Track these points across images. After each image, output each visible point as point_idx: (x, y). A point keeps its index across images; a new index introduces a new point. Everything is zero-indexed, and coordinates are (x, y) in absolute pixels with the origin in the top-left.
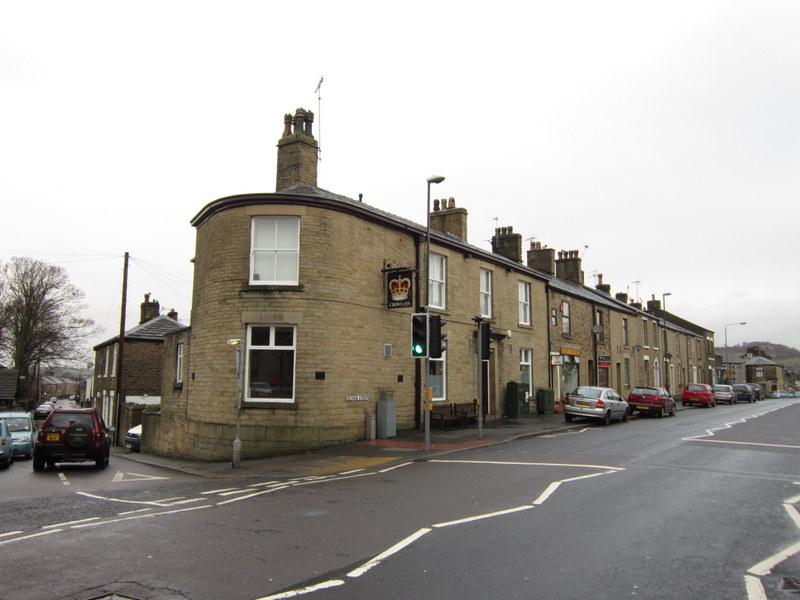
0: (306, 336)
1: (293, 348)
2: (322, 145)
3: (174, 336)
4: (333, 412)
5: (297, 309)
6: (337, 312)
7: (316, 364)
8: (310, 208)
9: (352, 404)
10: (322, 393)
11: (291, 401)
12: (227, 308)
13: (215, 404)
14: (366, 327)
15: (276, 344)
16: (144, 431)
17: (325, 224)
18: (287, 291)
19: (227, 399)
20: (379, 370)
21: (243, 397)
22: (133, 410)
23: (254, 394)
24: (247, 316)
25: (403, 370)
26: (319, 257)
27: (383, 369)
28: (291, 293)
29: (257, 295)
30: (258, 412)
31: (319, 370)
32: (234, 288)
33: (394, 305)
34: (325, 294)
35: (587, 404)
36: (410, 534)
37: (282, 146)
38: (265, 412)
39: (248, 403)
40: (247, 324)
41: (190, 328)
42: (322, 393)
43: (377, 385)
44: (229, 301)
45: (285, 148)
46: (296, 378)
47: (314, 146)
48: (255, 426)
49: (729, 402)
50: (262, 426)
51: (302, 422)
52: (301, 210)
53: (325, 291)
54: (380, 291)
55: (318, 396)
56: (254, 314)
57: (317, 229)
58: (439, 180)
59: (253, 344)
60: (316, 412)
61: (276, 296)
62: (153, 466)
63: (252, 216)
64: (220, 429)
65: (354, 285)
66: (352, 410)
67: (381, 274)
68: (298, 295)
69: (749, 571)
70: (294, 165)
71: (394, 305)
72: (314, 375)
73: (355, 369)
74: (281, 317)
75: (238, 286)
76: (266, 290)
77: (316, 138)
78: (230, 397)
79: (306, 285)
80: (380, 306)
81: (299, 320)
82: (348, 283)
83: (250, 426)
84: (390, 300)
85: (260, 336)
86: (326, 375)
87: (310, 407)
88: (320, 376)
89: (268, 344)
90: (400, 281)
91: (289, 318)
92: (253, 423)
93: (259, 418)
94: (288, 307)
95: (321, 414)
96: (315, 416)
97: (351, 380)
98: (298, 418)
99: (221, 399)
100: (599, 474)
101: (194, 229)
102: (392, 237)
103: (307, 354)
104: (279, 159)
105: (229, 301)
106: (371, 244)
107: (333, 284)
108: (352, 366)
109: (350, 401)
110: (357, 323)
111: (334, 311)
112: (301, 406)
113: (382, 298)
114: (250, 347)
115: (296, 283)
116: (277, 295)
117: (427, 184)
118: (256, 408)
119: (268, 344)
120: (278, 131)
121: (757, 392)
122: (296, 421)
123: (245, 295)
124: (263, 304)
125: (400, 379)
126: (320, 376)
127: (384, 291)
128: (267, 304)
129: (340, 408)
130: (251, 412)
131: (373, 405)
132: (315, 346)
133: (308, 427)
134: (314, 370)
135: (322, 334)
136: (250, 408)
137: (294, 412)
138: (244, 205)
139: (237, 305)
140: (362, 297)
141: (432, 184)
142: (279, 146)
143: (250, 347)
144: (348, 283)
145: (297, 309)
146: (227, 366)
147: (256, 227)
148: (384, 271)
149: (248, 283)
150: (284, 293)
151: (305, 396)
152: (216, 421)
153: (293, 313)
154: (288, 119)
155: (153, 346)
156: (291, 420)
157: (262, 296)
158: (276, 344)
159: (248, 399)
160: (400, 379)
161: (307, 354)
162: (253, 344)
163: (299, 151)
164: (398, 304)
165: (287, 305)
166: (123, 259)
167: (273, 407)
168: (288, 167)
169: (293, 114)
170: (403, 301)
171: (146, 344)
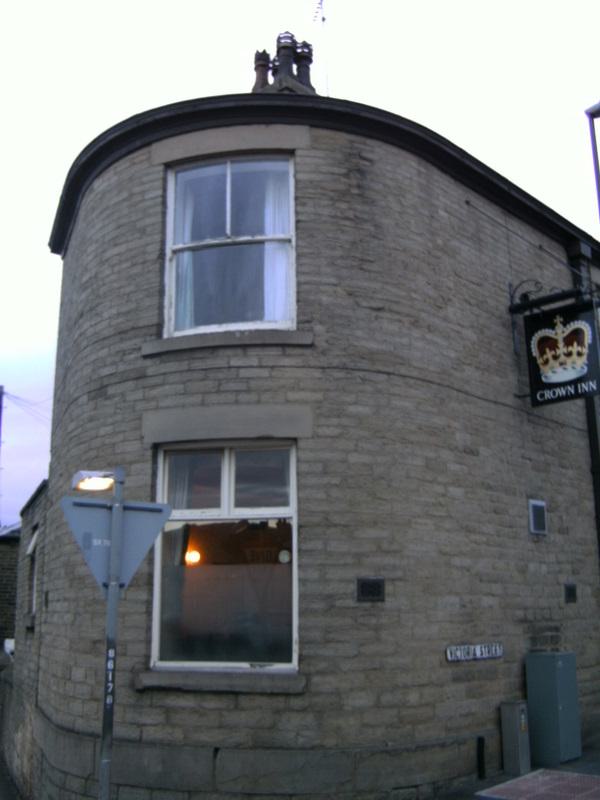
1: (289, 512)
6: (407, 404)
7: (359, 556)
9: (466, 673)
10: (378, 640)
13: (78, 674)
14: (483, 450)
15: (239, 503)
17: (361, 172)
20: (523, 571)
21: (148, 657)
25: (575, 572)
27: (532, 567)
31: (368, 574)
32: (124, 353)
33: (548, 394)
41: (280, 563)
42: (378, 640)
43: (520, 613)
46: (302, 597)
50: (203, 746)
52: (294, 135)
53: (373, 346)
54: (508, 359)
60: (362, 700)
65: (447, 338)
66: (462, 687)
67: (507, 316)
69: (171, 518)
71: (548, 394)
72: (353, 588)
73: (461, 568)
80: (510, 400)
82: (430, 329)
84: (536, 382)
86: (388, 588)
88: (371, 590)
89: (216, 504)
90: (560, 332)
95: (378, 705)
97: (454, 599)
101: (58, 258)
102: (525, 238)
103: (330, 525)
106: (477, 240)
107: (394, 327)
108: (457, 561)
109: (457, 662)
110: (461, 438)
111: (396, 402)
113: (509, 382)
117: (586, 120)
119: (216, 504)
121: (66, 573)
125: (571, 593)
126: (371, 590)
127: (518, 364)
129: (430, 684)
131: (516, 667)
134: (352, 573)
139: (131, 397)
140: (470, 372)
144: (430, 329)
145: (292, 396)
148: (514, 310)
151: (328, 651)
158: (240, 503)
160: (571, 593)
164: (561, 392)
167: (231, 693)
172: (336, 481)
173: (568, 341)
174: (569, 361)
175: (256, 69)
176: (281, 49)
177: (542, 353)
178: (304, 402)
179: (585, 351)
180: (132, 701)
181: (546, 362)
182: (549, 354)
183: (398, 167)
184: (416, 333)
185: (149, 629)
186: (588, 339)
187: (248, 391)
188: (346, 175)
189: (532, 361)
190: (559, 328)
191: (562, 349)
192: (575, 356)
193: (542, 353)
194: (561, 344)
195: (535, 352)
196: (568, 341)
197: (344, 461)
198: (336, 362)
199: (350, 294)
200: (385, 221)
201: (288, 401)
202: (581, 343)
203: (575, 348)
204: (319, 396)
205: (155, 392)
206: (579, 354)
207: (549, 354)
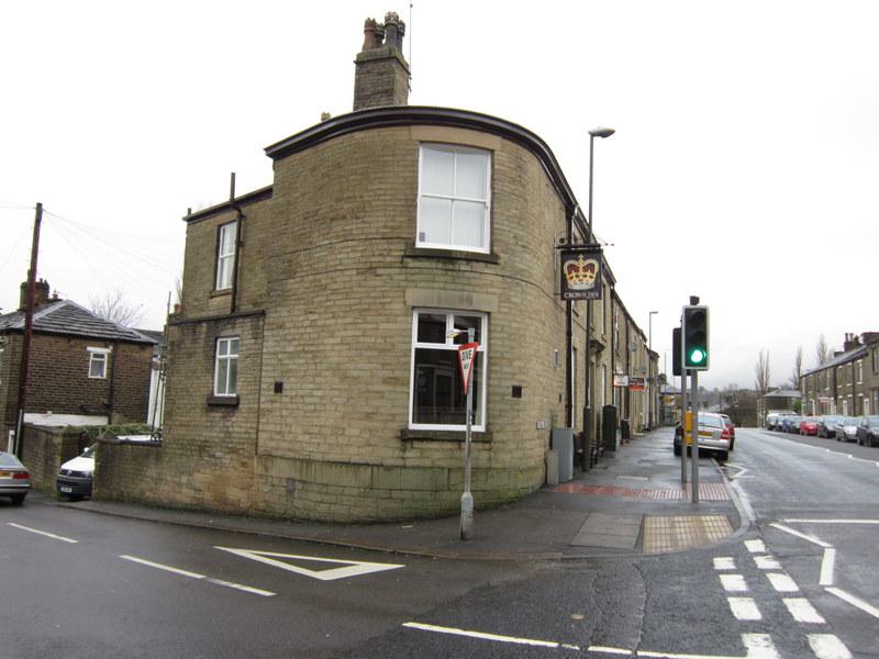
0: (502, 331)
2: (412, 70)
3: (204, 327)
4: (235, 435)
5: (491, 290)
7: (514, 374)
8: (507, 142)
11: (480, 428)
12: (378, 282)
15: (417, 350)
16: (101, 467)
18: (477, 261)
19: (376, 424)
22: (64, 435)
23: (417, 420)
24: (415, 295)
26: (515, 216)
28: (482, 265)
29: (433, 264)
30: (435, 445)
31: (516, 384)
34: (523, 270)
35: (709, 434)
36: (278, 568)
37: (361, 63)
38: (448, 446)
39: (414, 431)
40: (414, 308)
44: (379, 271)
45: (370, 67)
47: (405, 69)
48: (431, 468)
49: (849, 440)
50: (443, 468)
51: (497, 461)
52: (494, 141)
55: (516, 421)
56: (426, 292)
57: (514, 174)
58: (606, 134)
59: (419, 340)
61: (463, 268)
62: (156, 522)
63: (422, 142)
64: (365, 474)
68: (490, 269)
70: (386, 91)
72: (511, 390)
74: (470, 301)
75: (398, 249)
76: (446, 257)
77: (407, 59)
78: (387, 421)
79: (502, 255)
81: (493, 308)
83: (423, 468)
85: (431, 328)
87: (505, 438)
90: (581, 263)
91: (483, 301)
92: (428, 463)
93: (437, 455)
94: (478, 285)
95: (517, 448)
96: (510, 451)
98: (492, 454)
99: (367, 424)
100: (788, 521)
103: (504, 358)
104: (358, 81)
105: (379, 271)
112: (497, 436)
114: (416, 344)
115: (485, 250)
116: (463, 266)
117: (589, 136)
118: (432, 440)
120: (357, 42)
122: (490, 459)
123: (411, 263)
124: (442, 278)
126: (517, 392)
128: (448, 279)
130: (424, 445)
132: (512, 348)
133: (504, 469)
135: (518, 329)
136: (422, 440)
137: (487, 446)
138: (409, 124)
141: (595, 138)
142: (357, 63)
143: (416, 344)
145: (491, 290)
146: (381, 374)
147: (424, 155)
149: (414, 244)
150: (474, 264)
152: (355, 459)
153: (485, 294)
154: (371, 26)
155: (62, 343)
156: (482, 456)
157: (440, 265)
159: (413, 426)
161: (504, 358)
162: (419, 340)
163: (393, 72)
165: (479, 282)
166: (34, 212)
168: (375, 94)
169: (381, 21)
170: (587, 291)
171: (51, 339)
172: (506, 336)
173: (585, 269)
174: (585, 280)
175: (365, 32)
176: (387, 19)
177: (570, 273)
178: (494, 294)
179: (594, 276)
180: (399, 445)
181: (572, 278)
182: (574, 274)
183: (534, 166)
184: (535, 260)
185: (488, 402)
186: (596, 270)
187: (469, 285)
188: (516, 169)
189: (563, 276)
190: (581, 261)
191: (581, 273)
192: (588, 278)
193: (570, 273)
194: (581, 270)
195: (566, 272)
196: (585, 269)
197: (510, 326)
198: (508, 274)
199: (515, 237)
200: (528, 198)
201: (487, 293)
202: (592, 271)
203: (589, 273)
204: (501, 291)
205: (413, 278)
206: (591, 277)
207: (574, 274)
